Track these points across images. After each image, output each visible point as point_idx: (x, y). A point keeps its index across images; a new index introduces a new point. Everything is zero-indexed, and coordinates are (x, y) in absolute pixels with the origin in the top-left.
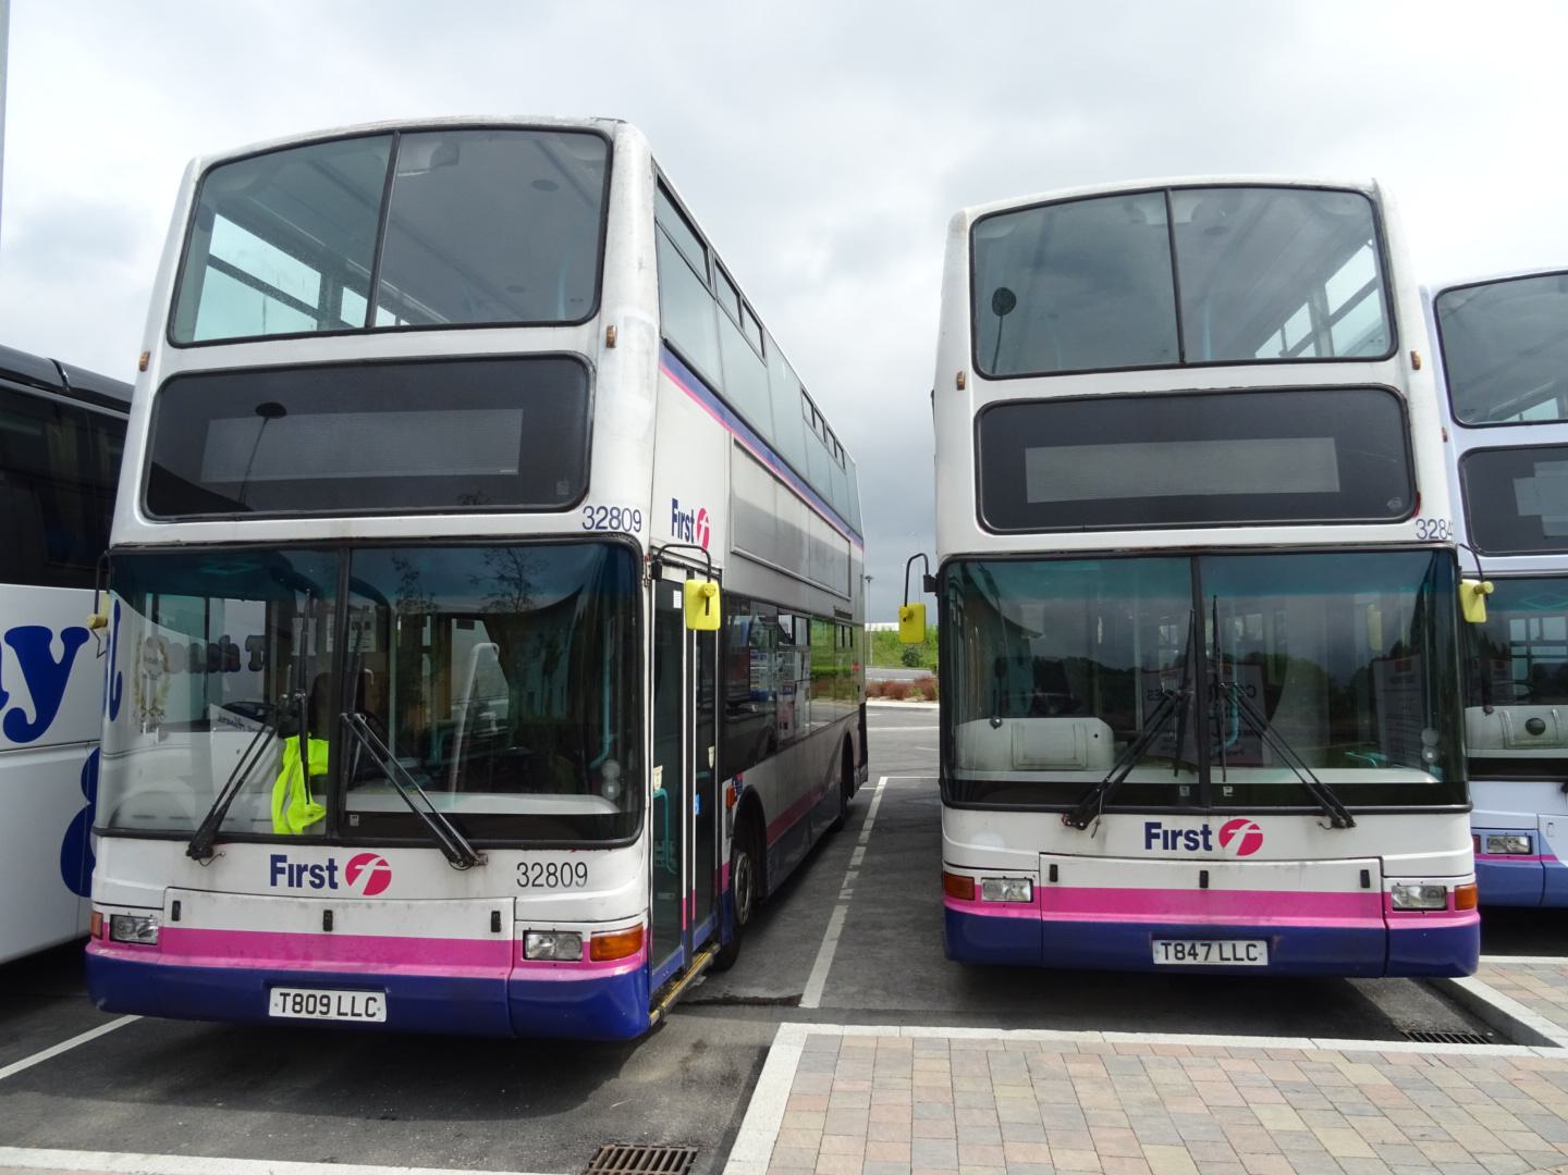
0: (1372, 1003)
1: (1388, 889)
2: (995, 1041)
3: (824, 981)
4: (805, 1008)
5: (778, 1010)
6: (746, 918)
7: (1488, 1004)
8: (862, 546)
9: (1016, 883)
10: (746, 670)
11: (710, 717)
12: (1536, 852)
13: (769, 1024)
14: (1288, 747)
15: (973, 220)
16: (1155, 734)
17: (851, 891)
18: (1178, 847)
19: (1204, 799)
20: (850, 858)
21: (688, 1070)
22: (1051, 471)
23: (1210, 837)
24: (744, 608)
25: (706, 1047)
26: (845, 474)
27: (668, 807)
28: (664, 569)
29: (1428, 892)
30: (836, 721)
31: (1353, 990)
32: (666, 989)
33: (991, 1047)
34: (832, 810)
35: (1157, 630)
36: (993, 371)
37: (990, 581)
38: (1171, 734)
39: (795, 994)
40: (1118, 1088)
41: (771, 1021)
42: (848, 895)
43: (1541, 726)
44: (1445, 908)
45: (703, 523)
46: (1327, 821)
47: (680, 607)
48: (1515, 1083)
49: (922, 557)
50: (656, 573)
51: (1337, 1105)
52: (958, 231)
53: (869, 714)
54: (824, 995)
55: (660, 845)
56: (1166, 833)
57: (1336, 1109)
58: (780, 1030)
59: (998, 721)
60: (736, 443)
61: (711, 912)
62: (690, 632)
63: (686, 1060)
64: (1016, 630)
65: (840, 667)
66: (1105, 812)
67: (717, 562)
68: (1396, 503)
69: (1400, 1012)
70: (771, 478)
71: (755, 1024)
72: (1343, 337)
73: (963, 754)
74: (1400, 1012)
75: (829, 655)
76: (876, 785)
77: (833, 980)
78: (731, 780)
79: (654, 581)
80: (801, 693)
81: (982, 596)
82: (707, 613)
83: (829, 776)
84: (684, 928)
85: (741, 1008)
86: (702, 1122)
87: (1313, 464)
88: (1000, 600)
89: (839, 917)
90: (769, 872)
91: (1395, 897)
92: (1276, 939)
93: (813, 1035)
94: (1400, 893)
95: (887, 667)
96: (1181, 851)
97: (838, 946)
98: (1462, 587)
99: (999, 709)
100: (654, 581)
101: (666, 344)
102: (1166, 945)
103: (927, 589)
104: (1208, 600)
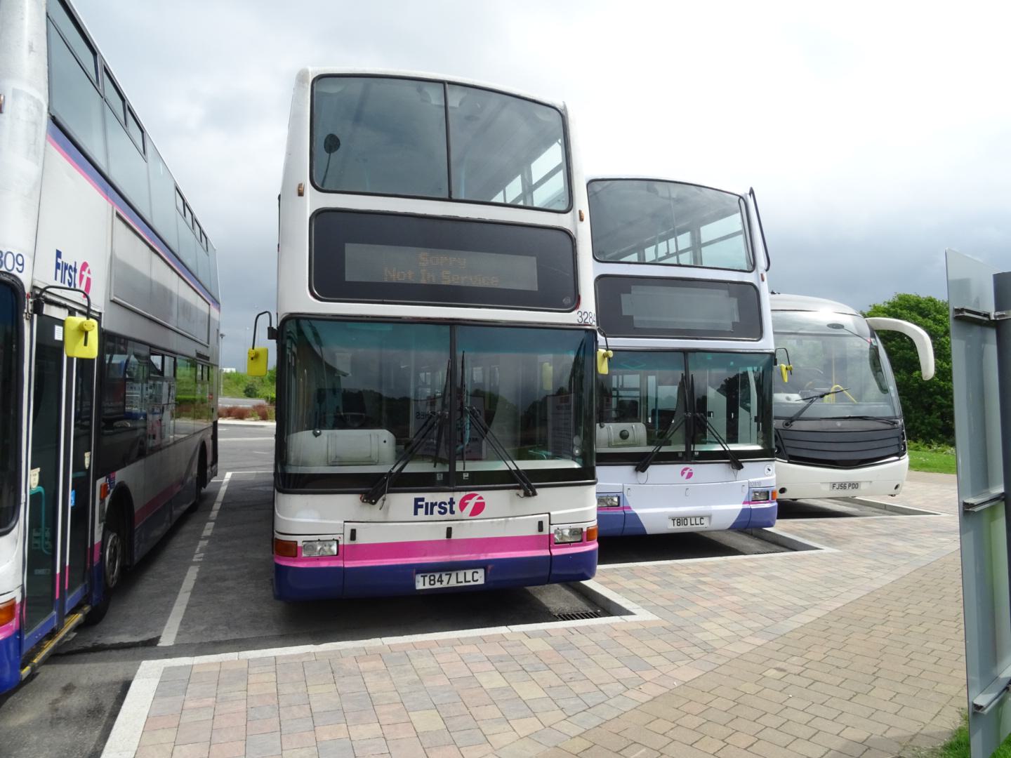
0: (537, 599)
1: (552, 532)
2: (308, 654)
3: (178, 624)
4: (162, 647)
5: (140, 651)
6: (115, 582)
7: (598, 593)
8: (219, 309)
9: (327, 543)
10: (122, 395)
11: (86, 431)
12: (621, 506)
13: (132, 663)
14: (502, 447)
15: (315, 76)
16: (423, 440)
17: (202, 555)
18: (434, 513)
19: (451, 481)
20: (203, 531)
21: (57, 710)
22: (361, 260)
23: (454, 505)
24: (122, 348)
25: (75, 687)
26: (208, 255)
27: (44, 506)
28: (45, 306)
29: (574, 532)
30: (195, 433)
31: (528, 593)
32: (39, 646)
33: (305, 659)
34: (189, 495)
35: (425, 375)
36: (323, 185)
37: (316, 334)
38: (432, 440)
39: (155, 637)
40: (393, 676)
41: (133, 660)
42: (200, 558)
43: (627, 434)
44: (581, 541)
45: (85, 274)
46: (521, 492)
47: (61, 339)
48: (615, 639)
49: (267, 314)
50: (38, 308)
51: (523, 666)
52: (303, 83)
53: (219, 429)
54: (179, 634)
55: (38, 531)
56: (427, 504)
57: (524, 669)
58: (141, 668)
59: (318, 432)
60: (118, 215)
61: (83, 581)
62: (70, 360)
63: (57, 701)
64: (332, 370)
65: (198, 397)
66: (388, 493)
67: (98, 307)
68: (567, 301)
69: (553, 603)
70: (148, 248)
71: (119, 664)
72: (540, 198)
73: (293, 455)
74: (553, 603)
75: (190, 388)
76: (223, 478)
77: (185, 623)
78: (104, 478)
79: (35, 316)
80: (167, 414)
81: (309, 345)
82: (86, 344)
83: (188, 473)
84: (57, 597)
85: (107, 653)
86: (67, 751)
87: (521, 272)
88: (323, 348)
89: (192, 575)
90: (136, 546)
91: (556, 536)
92: (490, 567)
93: (169, 668)
94: (558, 533)
95: (233, 397)
96: (436, 515)
97: (191, 596)
98: (598, 352)
99: (318, 423)
100: (35, 316)
101: (54, 120)
102: (424, 577)
103: (270, 337)
104: (459, 354)
